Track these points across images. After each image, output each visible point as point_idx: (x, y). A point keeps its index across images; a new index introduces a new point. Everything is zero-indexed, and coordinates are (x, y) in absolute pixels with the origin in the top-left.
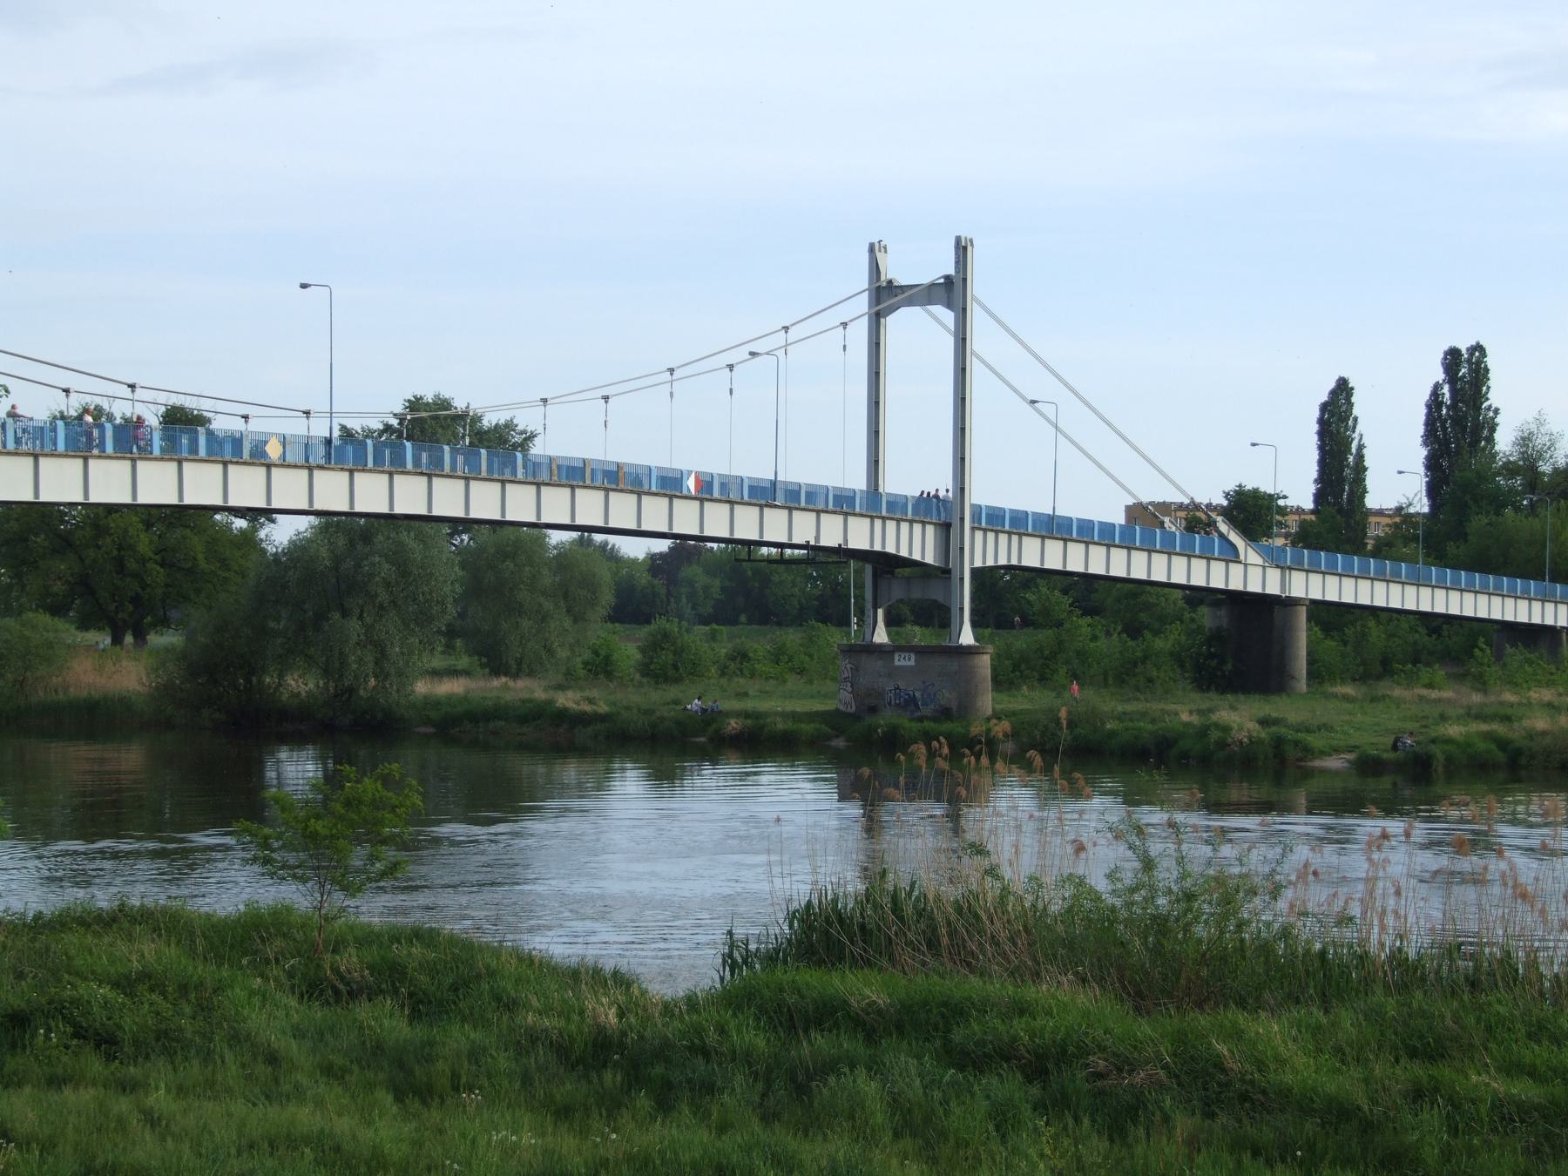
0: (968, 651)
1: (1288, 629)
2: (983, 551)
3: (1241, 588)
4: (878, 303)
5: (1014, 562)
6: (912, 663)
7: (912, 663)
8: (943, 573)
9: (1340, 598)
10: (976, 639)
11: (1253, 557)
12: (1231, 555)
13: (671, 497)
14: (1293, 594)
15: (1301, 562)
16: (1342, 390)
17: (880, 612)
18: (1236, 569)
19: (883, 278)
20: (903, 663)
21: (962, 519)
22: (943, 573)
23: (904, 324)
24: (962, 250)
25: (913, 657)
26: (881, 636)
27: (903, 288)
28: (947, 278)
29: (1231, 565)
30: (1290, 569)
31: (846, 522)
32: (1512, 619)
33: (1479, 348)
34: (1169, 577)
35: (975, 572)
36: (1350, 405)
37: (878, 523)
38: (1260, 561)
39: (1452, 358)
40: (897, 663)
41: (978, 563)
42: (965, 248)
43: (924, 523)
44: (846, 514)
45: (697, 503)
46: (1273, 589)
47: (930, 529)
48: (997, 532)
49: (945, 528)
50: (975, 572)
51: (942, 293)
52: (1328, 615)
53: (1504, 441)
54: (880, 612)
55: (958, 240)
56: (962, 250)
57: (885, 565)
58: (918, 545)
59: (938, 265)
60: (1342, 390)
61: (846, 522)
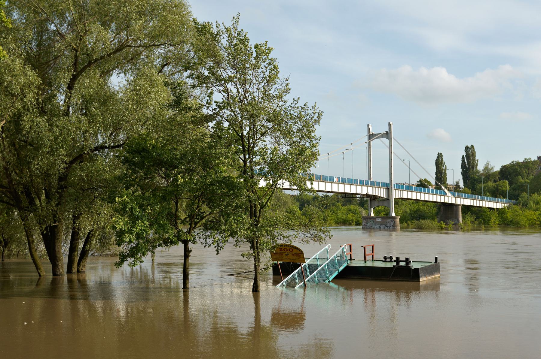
0: (394, 218)
1: (457, 211)
2: (396, 194)
3: (451, 203)
4: (370, 139)
5: (402, 197)
6: (381, 220)
7: (381, 220)
8: (388, 200)
9: (425, 199)
10: (396, 215)
11: (450, 195)
12: (445, 195)
13: (338, 184)
14: (458, 203)
15: (459, 196)
16: (440, 156)
17: (372, 209)
18: (446, 198)
19: (371, 132)
20: (378, 221)
21: (392, 187)
22: (388, 200)
23: (375, 142)
24: (390, 125)
25: (381, 219)
26: (372, 215)
27: (376, 135)
28: (387, 132)
29: (445, 197)
30: (457, 197)
31: (332, 184)
32: (443, 202)
33: (472, 146)
34: (433, 200)
35: (394, 199)
36: (442, 159)
37: (374, 188)
38: (451, 196)
39: (467, 148)
40: (377, 221)
41: (395, 198)
42: (391, 125)
43: (383, 188)
44: (319, 181)
45: (337, 184)
46: (454, 202)
47: (385, 189)
48: (398, 190)
49: (388, 189)
50: (394, 199)
51: (385, 135)
52: (466, 208)
53: (480, 167)
54: (372, 209)
55: (389, 123)
56: (390, 125)
57: (373, 198)
58: (381, 193)
59: (384, 129)
60: (440, 156)
61: (332, 184)
